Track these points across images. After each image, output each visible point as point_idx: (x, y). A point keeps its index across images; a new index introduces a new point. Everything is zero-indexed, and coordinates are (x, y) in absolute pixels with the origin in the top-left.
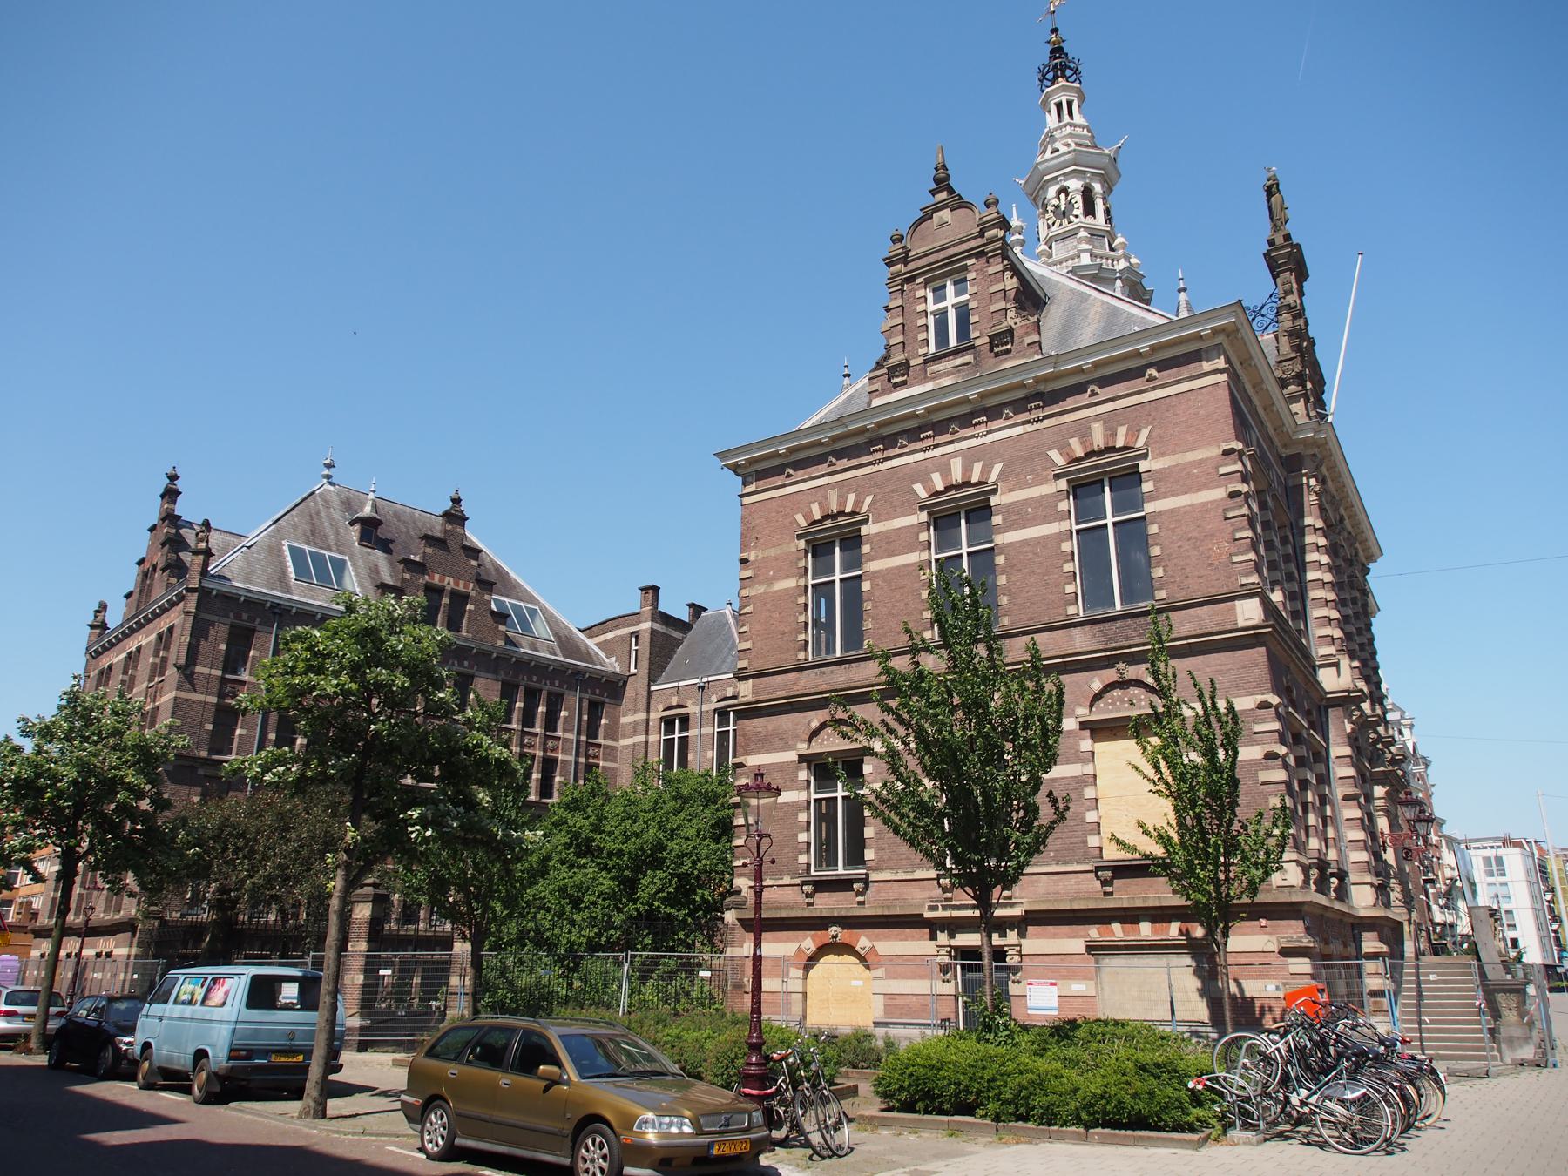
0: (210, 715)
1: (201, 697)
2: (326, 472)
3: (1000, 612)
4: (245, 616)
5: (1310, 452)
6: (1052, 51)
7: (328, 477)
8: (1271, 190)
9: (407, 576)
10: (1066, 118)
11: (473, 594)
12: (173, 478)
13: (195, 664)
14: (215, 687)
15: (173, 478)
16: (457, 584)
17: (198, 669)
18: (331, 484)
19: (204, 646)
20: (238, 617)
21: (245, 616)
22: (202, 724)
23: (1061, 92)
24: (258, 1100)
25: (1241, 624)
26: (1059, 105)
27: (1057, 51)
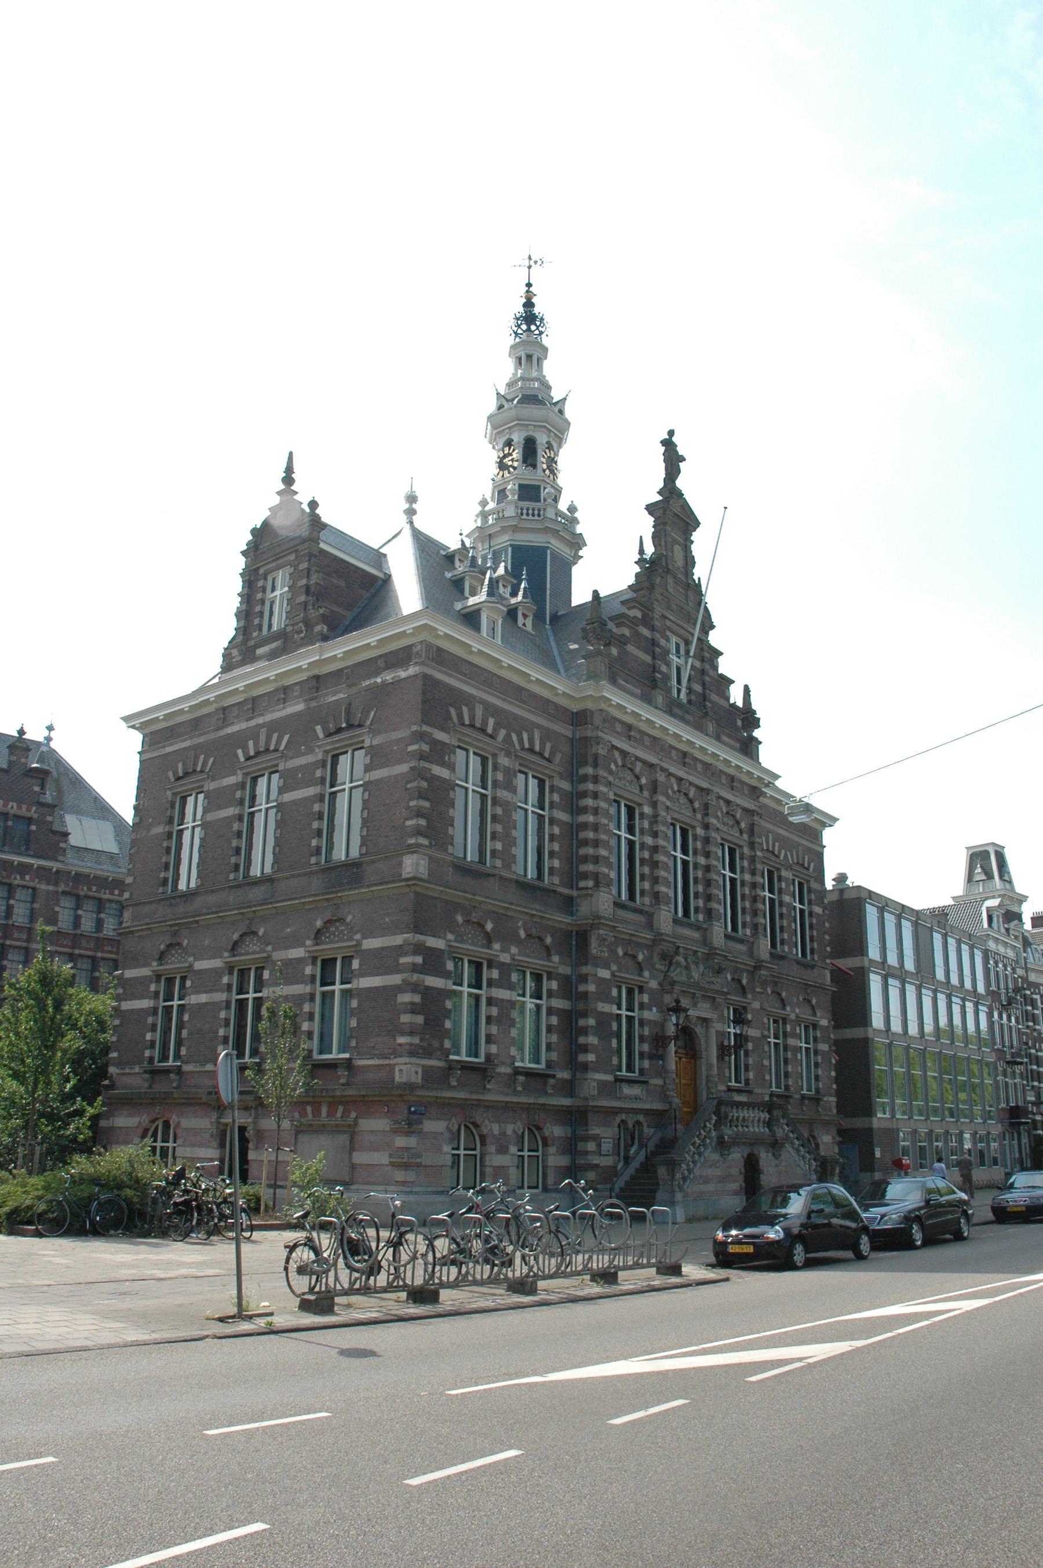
8: (668, 444)
11: (35, 816)
16: (19, 807)
25: (404, 876)
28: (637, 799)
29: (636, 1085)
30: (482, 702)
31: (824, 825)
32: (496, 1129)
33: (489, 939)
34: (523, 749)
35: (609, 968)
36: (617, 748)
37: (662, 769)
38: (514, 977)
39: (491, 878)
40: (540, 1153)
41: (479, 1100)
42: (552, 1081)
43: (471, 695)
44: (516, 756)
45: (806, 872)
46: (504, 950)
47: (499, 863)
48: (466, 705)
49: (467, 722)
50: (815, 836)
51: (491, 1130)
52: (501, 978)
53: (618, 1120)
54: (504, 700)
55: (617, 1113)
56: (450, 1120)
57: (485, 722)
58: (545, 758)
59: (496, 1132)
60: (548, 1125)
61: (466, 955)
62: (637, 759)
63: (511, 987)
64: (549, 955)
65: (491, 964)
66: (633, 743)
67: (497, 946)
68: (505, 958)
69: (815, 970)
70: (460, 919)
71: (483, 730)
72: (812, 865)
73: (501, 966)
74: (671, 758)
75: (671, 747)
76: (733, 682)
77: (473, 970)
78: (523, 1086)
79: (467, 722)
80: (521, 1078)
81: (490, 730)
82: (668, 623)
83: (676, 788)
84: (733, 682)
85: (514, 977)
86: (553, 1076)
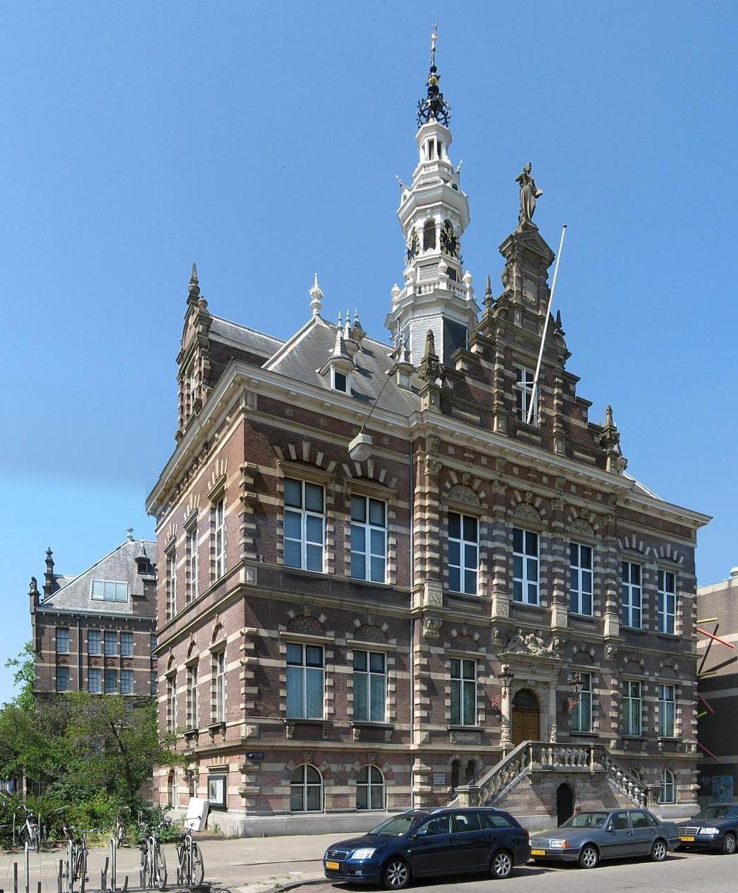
0: (54, 673)
1: (48, 665)
2: (129, 534)
3: (151, 586)
4: (62, 623)
5: (427, 433)
6: (430, 89)
7: (130, 537)
9: (147, 589)
10: (436, 157)
12: (50, 553)
13: (41, 649)
14: (54, 659)
15: (50, 553)
17: (43, 652)
18: (132, 540)
19: (44, 640)
20: (59, 623)
21: (62, 623)
22: (51, 677)
23: (430, 130)
24: (519, 876)
26: (431, 143)
27: (433, 90)
28: (538, 527)
29: (470, 734)
30: (309, 439)
31: (698, 524)
32: (648, 771)
33: (642, 669)
34: (660, 558)
35: (442, 646)
36: (572, 506)
37: (502, 484)
38: (657, 689)
39: (325, 582)
40: (322, 785)
41: (316, 748)
42: (645, 743)
43: (296, 435)
44: (657, 562)
45: (641, 556)
46: (652, 675)
47: (647, 626)
48: (293, 444)
49: (294, 457)
50: (688, 534)
51: (645, 773)
52: (683, 694)
53: (452, 759)
54: (333, 437)
55: (450, 755)
56: (288, 762)
57: (638, 545)
58: (380, 483)
59: (648, 773)
60: (643, 768)
61: (462, 657)
62: (590, 512)
63: (656, 695)
64: (677, 675)
65: (677, 687)
66: (467, 463)
67: (647, 673)
68: (652, 679)
69: (680, 643)
70: (626, 660)
71: (671, 559)
72: (682, 558)
73: (650, 683)
74: (513, 475)
75: (543, 474)
76: (591, 404)
77: (668, 690)
78: (628, 746)
79: (294, 457)
80: (627, 742)
81: (641, 549)
82: (515, 355)
83: (576, 516)
84: (591, 404)
85: (657, 689)
86: (646, 741)
